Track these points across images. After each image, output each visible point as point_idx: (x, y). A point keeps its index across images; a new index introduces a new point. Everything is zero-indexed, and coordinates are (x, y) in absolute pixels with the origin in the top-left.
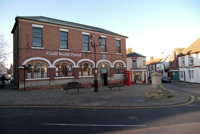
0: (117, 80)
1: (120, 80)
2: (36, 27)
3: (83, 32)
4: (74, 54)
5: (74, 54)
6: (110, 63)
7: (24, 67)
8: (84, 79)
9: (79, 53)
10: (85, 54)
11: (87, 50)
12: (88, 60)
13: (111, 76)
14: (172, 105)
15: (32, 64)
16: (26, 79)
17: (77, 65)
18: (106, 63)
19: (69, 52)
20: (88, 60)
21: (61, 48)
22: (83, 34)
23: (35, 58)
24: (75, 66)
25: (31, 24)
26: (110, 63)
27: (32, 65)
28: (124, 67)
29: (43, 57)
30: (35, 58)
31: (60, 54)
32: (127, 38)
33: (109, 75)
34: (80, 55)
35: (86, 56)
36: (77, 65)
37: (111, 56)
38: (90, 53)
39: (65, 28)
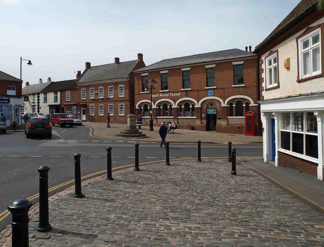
3: (206, 65)
6: (221, 101)
9: (178, 92)
10: (185, 93)
12: (189, 99)
14: (128, 167)
17: (176, 104)
18: (216, 102)
19: (168, 92)
20: (189, 99)
24: (223, 105)
25: (180, 68)
26: (196, 102)
28: (250, 105)
31: (161, 95)
33: (218, 116)
34: (179, 94)
35: (186, 94)
36: (176, 104)
38: (191, 91)
39: (186, 67)
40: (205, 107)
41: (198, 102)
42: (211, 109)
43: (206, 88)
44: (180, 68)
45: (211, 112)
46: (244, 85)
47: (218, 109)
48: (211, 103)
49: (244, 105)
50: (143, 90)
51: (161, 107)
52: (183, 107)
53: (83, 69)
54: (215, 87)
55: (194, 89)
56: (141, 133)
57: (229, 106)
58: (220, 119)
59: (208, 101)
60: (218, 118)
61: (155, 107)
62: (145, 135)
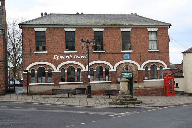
0: (150, 87)
1: (155, 88)
2: (42, 30)
3: (122, 28)
4: (77, 57)
5: (77, 57)
6: (138, 64)
7: (26, 72)
8: (96, 85)
11: (155, 48)
13: (141, 81)
15: (36, 69)
16: (30, 84)
18: (131, 65)
21: (150, 48)
22: (94, 30)
23: (151, 61)
24: (139, 69)
27: (35, 70)
29: (46, 62)
30: (151, 61)
31: (64, 57)
32: (171, 25)
35: (99, 57)
36: (142, 67)
37: (139, 55)
38: (105, 53)
39: (125, 28)
40: (120, 69)
41: (113, 66)
42: (127, 72)
43: (121, 51)
44: (146, 28)
45: (128, 75)
46: (104, 51)
47: (134, 73)
48: (127, 68)
49: (76, 71)
50: (38, 49)
51: (66, 71)
52: (36, 72)
53: (80, 13)
54: (132, 51)
55: (108, 51)
56: (136, 99)
57: (61, 71)
58: (136, 82)
59: (124, 65)
60: (134, 81)
61: (142, 69)
62: (140, 102)
